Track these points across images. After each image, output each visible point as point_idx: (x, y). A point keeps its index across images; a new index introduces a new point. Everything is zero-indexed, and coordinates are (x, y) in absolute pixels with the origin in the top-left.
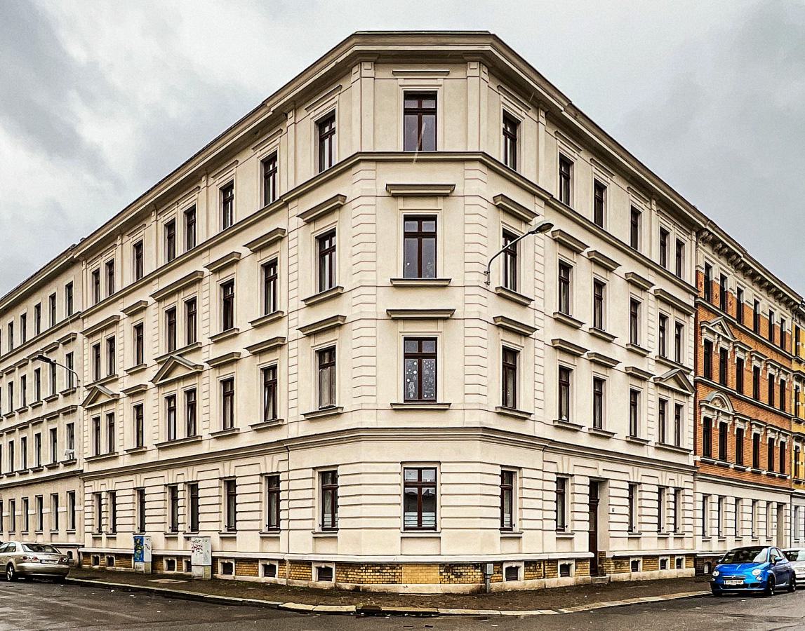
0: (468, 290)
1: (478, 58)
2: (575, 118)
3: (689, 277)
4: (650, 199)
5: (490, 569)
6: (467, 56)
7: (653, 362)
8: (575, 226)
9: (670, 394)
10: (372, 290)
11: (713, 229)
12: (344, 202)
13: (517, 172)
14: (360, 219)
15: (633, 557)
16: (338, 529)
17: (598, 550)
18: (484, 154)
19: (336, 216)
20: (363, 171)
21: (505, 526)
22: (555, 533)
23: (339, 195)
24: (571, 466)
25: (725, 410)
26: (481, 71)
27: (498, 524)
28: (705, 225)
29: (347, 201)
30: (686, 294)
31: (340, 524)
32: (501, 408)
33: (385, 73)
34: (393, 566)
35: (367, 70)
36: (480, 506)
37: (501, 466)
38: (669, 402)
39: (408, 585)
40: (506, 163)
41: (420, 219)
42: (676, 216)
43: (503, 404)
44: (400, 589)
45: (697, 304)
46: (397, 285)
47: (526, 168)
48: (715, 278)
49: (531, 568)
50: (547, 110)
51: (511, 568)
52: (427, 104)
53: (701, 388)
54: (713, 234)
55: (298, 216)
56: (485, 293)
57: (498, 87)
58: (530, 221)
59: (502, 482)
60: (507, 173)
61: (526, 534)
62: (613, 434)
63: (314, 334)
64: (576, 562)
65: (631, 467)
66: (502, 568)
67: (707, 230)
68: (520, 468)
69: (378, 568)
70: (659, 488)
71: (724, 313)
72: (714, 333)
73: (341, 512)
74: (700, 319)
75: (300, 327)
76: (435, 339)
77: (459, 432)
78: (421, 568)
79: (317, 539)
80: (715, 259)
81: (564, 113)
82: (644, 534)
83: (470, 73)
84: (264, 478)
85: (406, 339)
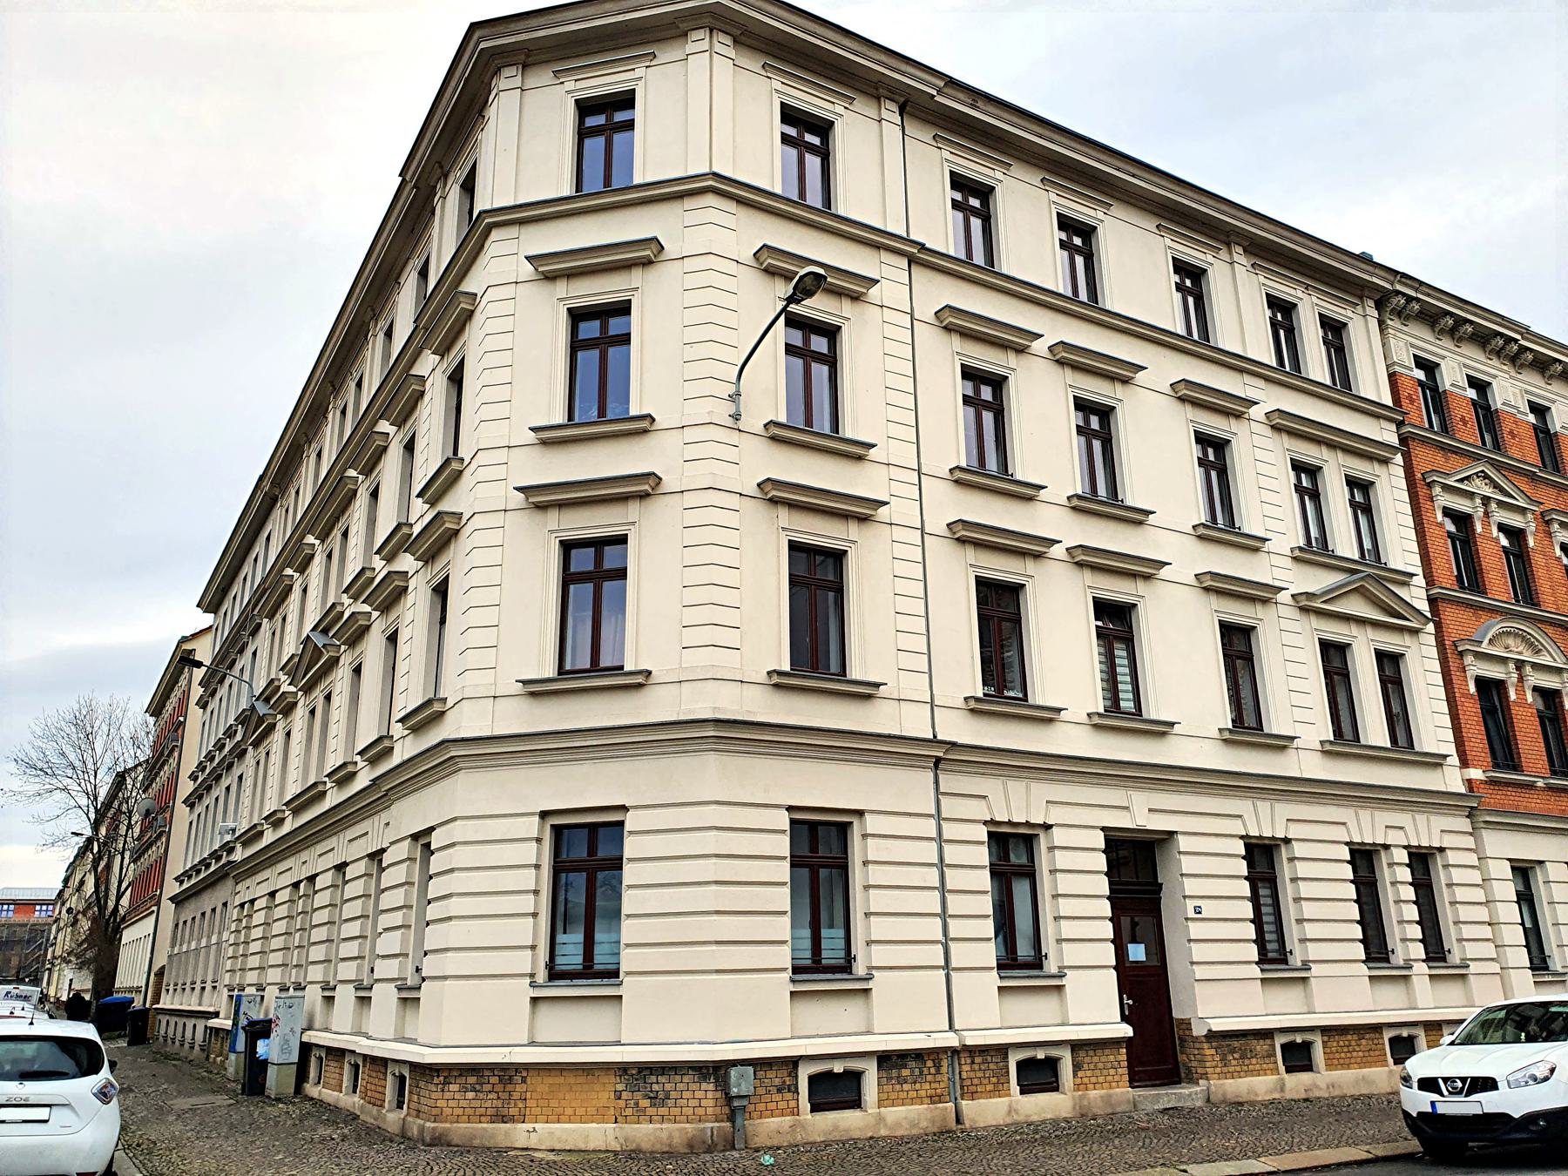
0: (690, 435)
1: (707, 20)
2: (973, 106)
3: (1371, 383)
4: (1361, 298)
5: (742, 1083)
6: (683, 22)
7: (1288, 563)
8: (1357, 416)
9: (1354, 630)
10: (502, 455)
11: (1416, 290)
12: (655, 256)
13: (1354, 393)
15: (1391, 1025)
17: (1175, 1015)
18: (715, 175)
20: (713, 210)
21: (1270, 955)
22: (1424, 964)
24: (1436, 832)
25: (1544, 659)
26: (715, 41)
27: (1253, 952)
30: (1236, 376)
32: (1331, 742)
34: (508, 1073)
35: (723, 44)
36: (718, 912)
37: (790, 809)
38: (1354, 646)
39: (537, 1126)
40: (1335, 384)
42: (1170, 216)
43: (1335, 735)
44: (520, 1134)
45: (1403, 440)
46: (550, 439)
47: (1226, 338)
48: (1452, 385)
49: (905, 1072)
50: (902, 100)
51: (829, 1075)
52: (620, 117)
53: (1450, 614)
54: (1418, 300)
56: (734, 437)
57: (1157, 226)
58: (1133, 378)
59: (1354, 871)
60: (1098, 316)
61: (880, 982)
62: (1172, 724)
64: (1073, 1051)
65: (1426, 815)
66: (1273, 1046)
67: (1398, 293)
68: (860, 813)
69: (472, 1080)
70: (1245, 844)
71: (1560, 477)
72: (1470, 495)
74: (1420, 467)
77: (1258, 782)
78: (572, 1080)
79: (409, 1003)
80: (1493, 367)
81: (939, 99)
82: (1316, 969)
83: (690, 47)
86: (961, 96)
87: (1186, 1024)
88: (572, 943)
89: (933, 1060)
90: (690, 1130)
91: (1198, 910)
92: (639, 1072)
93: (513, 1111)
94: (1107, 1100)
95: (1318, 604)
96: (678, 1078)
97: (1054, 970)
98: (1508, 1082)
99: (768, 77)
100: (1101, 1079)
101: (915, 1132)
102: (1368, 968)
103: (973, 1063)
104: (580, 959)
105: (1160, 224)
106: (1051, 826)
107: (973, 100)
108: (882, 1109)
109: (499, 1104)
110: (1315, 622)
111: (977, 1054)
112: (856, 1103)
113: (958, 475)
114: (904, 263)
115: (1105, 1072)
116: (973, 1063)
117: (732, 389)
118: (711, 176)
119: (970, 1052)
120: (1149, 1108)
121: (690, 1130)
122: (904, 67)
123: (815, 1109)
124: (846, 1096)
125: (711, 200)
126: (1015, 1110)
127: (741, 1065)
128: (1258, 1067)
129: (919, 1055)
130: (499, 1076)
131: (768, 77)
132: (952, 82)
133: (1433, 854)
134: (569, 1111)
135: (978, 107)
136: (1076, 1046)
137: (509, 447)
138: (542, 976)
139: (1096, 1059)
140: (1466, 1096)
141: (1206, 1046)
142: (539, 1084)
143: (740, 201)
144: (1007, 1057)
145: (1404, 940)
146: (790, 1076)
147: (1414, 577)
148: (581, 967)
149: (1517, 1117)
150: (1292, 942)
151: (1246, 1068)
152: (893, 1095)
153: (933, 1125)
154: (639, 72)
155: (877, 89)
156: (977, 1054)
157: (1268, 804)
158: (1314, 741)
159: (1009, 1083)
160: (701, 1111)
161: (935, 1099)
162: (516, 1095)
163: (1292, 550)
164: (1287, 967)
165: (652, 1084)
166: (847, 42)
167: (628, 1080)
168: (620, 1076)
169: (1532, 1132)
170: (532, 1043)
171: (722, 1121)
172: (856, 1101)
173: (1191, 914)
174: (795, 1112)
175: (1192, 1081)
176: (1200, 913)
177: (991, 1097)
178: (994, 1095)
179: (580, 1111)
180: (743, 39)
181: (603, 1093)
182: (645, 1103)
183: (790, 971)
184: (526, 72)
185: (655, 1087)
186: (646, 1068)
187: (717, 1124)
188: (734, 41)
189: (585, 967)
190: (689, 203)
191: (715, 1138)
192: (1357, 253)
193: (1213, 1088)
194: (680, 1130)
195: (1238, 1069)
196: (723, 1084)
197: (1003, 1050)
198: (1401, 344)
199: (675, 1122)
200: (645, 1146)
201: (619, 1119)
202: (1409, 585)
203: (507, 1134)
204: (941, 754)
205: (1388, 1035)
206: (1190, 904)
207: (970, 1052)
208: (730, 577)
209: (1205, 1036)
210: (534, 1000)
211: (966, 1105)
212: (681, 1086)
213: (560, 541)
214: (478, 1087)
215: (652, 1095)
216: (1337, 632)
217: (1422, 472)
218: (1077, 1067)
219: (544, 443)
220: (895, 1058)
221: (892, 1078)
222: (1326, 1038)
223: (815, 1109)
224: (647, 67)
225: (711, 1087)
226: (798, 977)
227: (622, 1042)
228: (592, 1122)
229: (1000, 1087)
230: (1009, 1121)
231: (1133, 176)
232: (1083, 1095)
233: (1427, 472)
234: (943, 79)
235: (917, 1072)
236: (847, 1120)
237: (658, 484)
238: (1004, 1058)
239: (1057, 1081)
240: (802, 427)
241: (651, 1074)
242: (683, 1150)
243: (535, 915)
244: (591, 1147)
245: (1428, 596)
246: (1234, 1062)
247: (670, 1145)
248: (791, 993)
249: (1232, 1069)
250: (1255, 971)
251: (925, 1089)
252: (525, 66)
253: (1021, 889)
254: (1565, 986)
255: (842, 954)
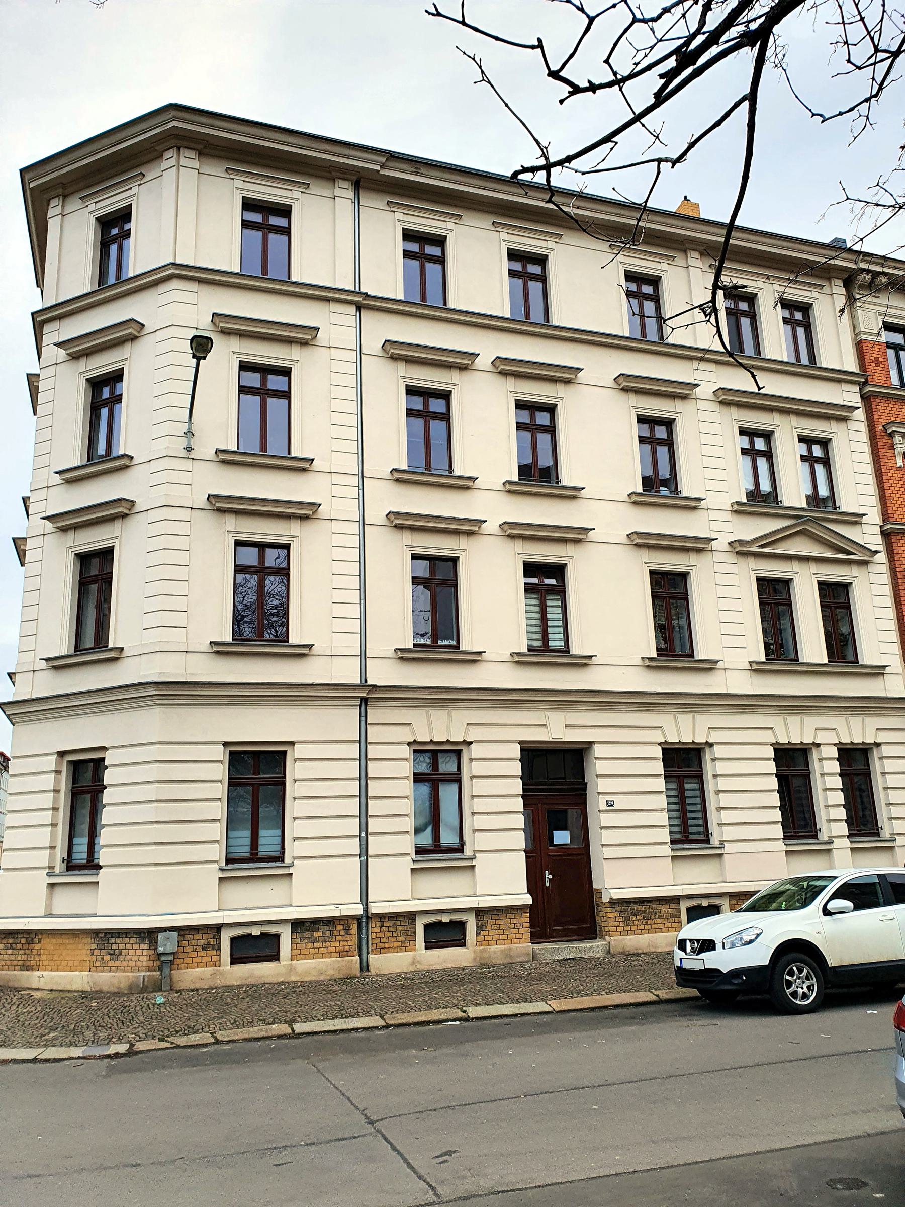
0: (336, 479)
2: (416, 173)
7: (728, 516)
9: (796, 566)
11: (882, 265)
12: (139, 332)
14: (167, 346)
16: (100, 867)
19: (126, 351)
20: (177, 291)
23: (133, 319)
28: (856, 262)
29: (146, 331)
31: (103, 857)
33: (216, 169)
34: (30, 936)
35: (189, 159)
37: (226, 744)
39: (45, 973)
41: (265, 370)
49: (318, 934)
55: (55, 345)
56: (188, 464)
61: (480, 862)
63: (60, 319)
67: (863, 270)
68: (292, 743)
69: (11, 941)
73: (105, 837)
75: (48, 514)
76: (287, 547)
83: (165, 164)
84: (65, 764)
85: (238, 543)
86: (405, 167)
87: (599, 891)
88: (243, 836)
89: (343, 925)
90: (131, 977)
91: (610, 803)
92: (105, 936)
93: (33, 963)
94: (507, 953)
95: (754, 549)
96: (127, 940)
97: (826, 839)
98: (723, 944)
99: (230, 178)
100: (503, 937)
101: (322, 978)
102: (785, 845)
103: (382, 926)
104: (248, 849)
105: (611, 244)
106: (471, 743)
107: (416, 168)
108: (294, 962)
109: (25, 957)
110: (752, 563)
111: (387, 919)
112: (275, 957)
113: (397, 475)
114: (353, 310)
115: (507, 932)
116: (382, 926)
117: (185, 427)
118: (171, 266)
119: (380, 918)
120: (549, 957)
121: (131, 977)
122: (346, 151)
123: (235, 961)
124: (268, 952)
125: (175, 284)
126: (418, 961)
127: (170, 931)
128: (661, 926)
129: (330, 922)
130: (26, 938)
131: (230, 178)
132: (393, 157)
133: (872, 748)
134: (64, 963)
135: (422, 173)
136: (480, 912)
137: (48, 487)
138: (59, 867)
139: (500, 922)
140: (697, 955)
141: (609, 910)
142: (48, 944)
143: (200, 281)
144: (415, 922)
145: (890, 819)
146: (214, 937)
147: (864, 517)
148: (86, 861)
149: (725, 972)
150: (713, 827)
151: (649, 927)
152: (304, 951)
153: (339, 973)
154: (134, 190)
155: (331, 173)
156: (387, 919)
157: (690, 716)
158: (744, 662)
159: (415, 941)
160: (139, 963)
161: (342, 954)
162: (35, 952)
163: (732, 505)
164: (879, 839)
165: (112, 944)
166: (290, 139)
167: (98, 941)
168: (94, 939)
169: (734, 984)
170: (50, 915)
171: (155, 971)
172: (274, 955)
173: (603, 806)
174: (218, 963)
175: (603, 937)
176: (612, 805)
177: (397, 952)
178: (400, 949)
179: (70, 963)
180: (207, 151)
181: (83, 950)
182: (107, 958)
183: (670, 843)
184: (66, 202)
185: (114, 947)
186: (109, 933)
187: (149, 973)
188: (199, 154)
189: (89, 861)
190: (162, 288)
191: (146, 984)
192: (827, 242)
193: (613, 943)
194: (125, 977)
195: (642, 927)
196: (153, 944)
197: (411, 916)
198: (871, 315)
199: (124, 972)
200: (105, 988)
201: (92, 968)
202: (861, 523)
203: (28, 977)
204: (365, 695)
205: (684, 906)
206: (602, 800)
207: (380, 918)
208: (182, 573)
209: (609, 902)
210: (52, 885)
211: (372, 958)
212: (128, 946)
213: (75, 554)
214: (14, 946)
215: (111, 952)
216: (775, 570)
217: (884, 424)
218: (480, 928)
219: (68, 482)
220: (309, 923)
221: (305, 939)
222: (733, 902)
223: (235, 961)
224: (139, 185)
225: (146, 946)
226: (420, 857)
227: (97, 914)
228: (77, 971)
229: (407, 944)
230: (411, 969)
231: (578, 208)
232: (484, 949)
233: (888, 424)
234: (383, 156)
235: (328, 934)
236: (263, 971)
237: (133, 506)
238: (217, 932)
239: (464, 939)
240: (258, 452)
241: (112, 938)
242: (126, 992)
243: (54, 825)
244: (74, 988)
245: (881, 532)
246: (636, 922)
247: (119, 988)
248: (412, 869)
249: (634, 928)
250: (781, 846)
251: (335, 946)
252: (65, 197)
253: (448, 792)
254: (474, 875)
255: (279, 848)
